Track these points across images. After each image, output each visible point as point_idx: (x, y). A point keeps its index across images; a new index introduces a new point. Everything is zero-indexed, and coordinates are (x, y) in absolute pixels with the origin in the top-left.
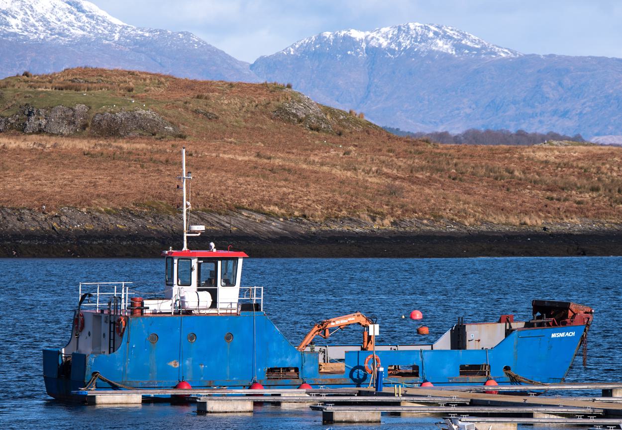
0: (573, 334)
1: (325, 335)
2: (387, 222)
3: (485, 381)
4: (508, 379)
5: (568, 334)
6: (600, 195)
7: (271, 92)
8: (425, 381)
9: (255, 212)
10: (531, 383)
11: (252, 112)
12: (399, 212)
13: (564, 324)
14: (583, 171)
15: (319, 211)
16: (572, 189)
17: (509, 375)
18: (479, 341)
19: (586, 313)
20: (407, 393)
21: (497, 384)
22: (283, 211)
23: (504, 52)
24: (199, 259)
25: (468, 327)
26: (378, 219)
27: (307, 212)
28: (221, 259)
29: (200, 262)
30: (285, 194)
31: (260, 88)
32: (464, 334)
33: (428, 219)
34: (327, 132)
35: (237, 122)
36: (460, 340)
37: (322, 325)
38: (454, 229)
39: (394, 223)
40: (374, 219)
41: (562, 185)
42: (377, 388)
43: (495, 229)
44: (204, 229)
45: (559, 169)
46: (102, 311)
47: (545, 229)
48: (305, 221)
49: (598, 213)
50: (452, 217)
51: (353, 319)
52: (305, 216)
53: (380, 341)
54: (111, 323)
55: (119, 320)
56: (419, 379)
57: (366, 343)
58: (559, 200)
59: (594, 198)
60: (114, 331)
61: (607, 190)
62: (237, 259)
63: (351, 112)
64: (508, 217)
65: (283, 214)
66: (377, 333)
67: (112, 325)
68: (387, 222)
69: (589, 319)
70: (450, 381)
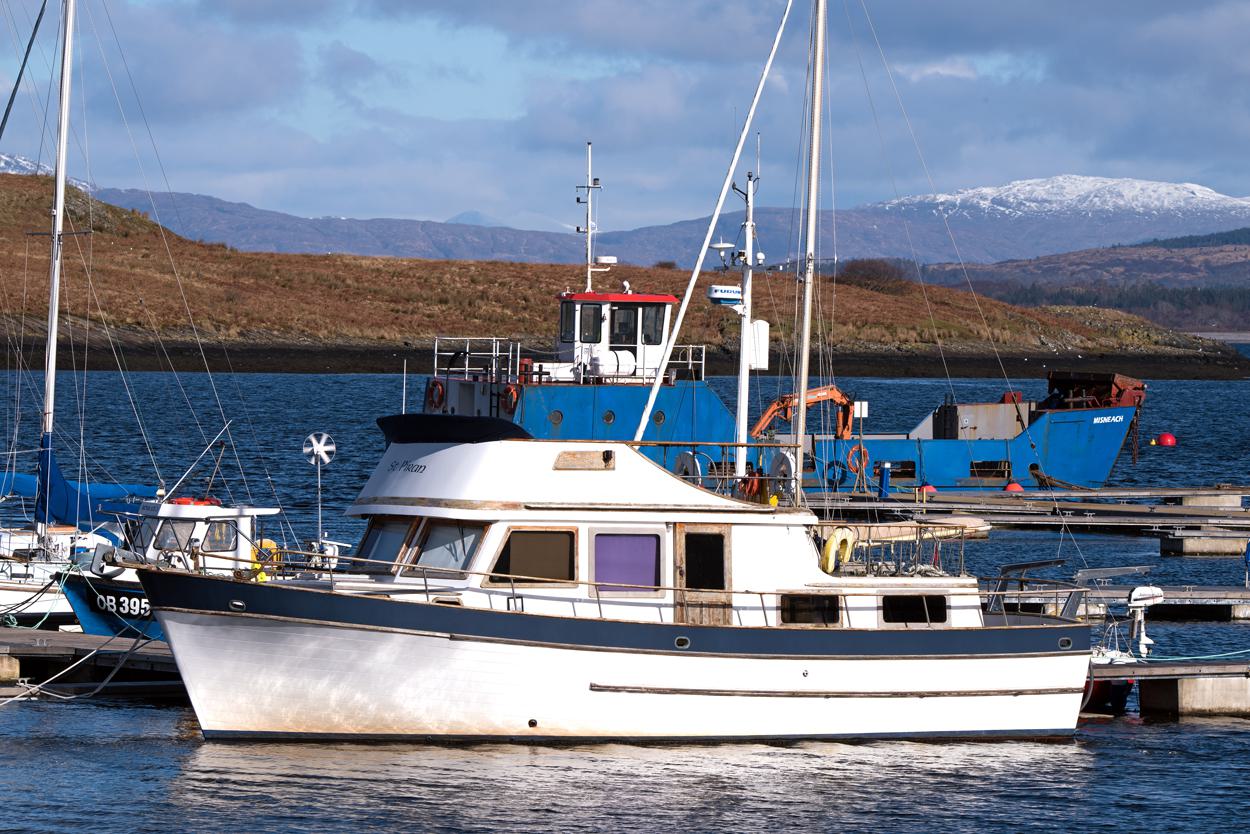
0: (1121, 418)
1: (786, 416)
2: (234, 331)
3: (1004, 484)
4: (1036, 482)
5: (1115, 419)
6: (450, 308)
7: (43, 184)
8: (925, 484)
9: (80, 317)
10: (1070, 488)
11: (22, 208)
12: (245, 321)
13: (1108, 404)
14: (422, 280)
15: (152, 318)
16: (418, 301)
17: (1037, 476)
18: (975, 428)
19: (1135, 389)
20: (934, 499)
21: (1022, 489)
22: (112, 317)
23: (83, 186)
24: (613, 304)
25: (961, 410)
26: (222, 329)
27: (140, 319)
28: (644, 305)
29: (615, 308)
30: (110, 297)
31: (30, 180)
32: (954, 419)
33: (278, 330)
34: (112, 233)
35: (5, 218)
36: (948, 427)
37: (783, 402)
38: (308, 342)
39: (241, 334)
40: (218, 329)
41: (406, 296)
42: (880, 492)
43: (354, 342)
44: (615, 261)
45: (395, 278)
46: (476, 379)
47: (406, 344)
48: (139, 328)
49: (453, 328)
50: (302, 328)
51: (825, 394)
52: (139, 324)
53: (868, 425)
54: (492, 394)
55: (508, 390)
56: (915, 481)
57: (840, 429)
58: (405, 312)
59: (444, 311)
60: (498, 407)
61: (458, 304)
62: (664, 305)
63: (133, 211)
64: (361, 331)
65: (113, 321)
66: (865, 414)
67: (495, 399)
68: (234, 331)
69: (1140, 397)
70: (958, 484)
